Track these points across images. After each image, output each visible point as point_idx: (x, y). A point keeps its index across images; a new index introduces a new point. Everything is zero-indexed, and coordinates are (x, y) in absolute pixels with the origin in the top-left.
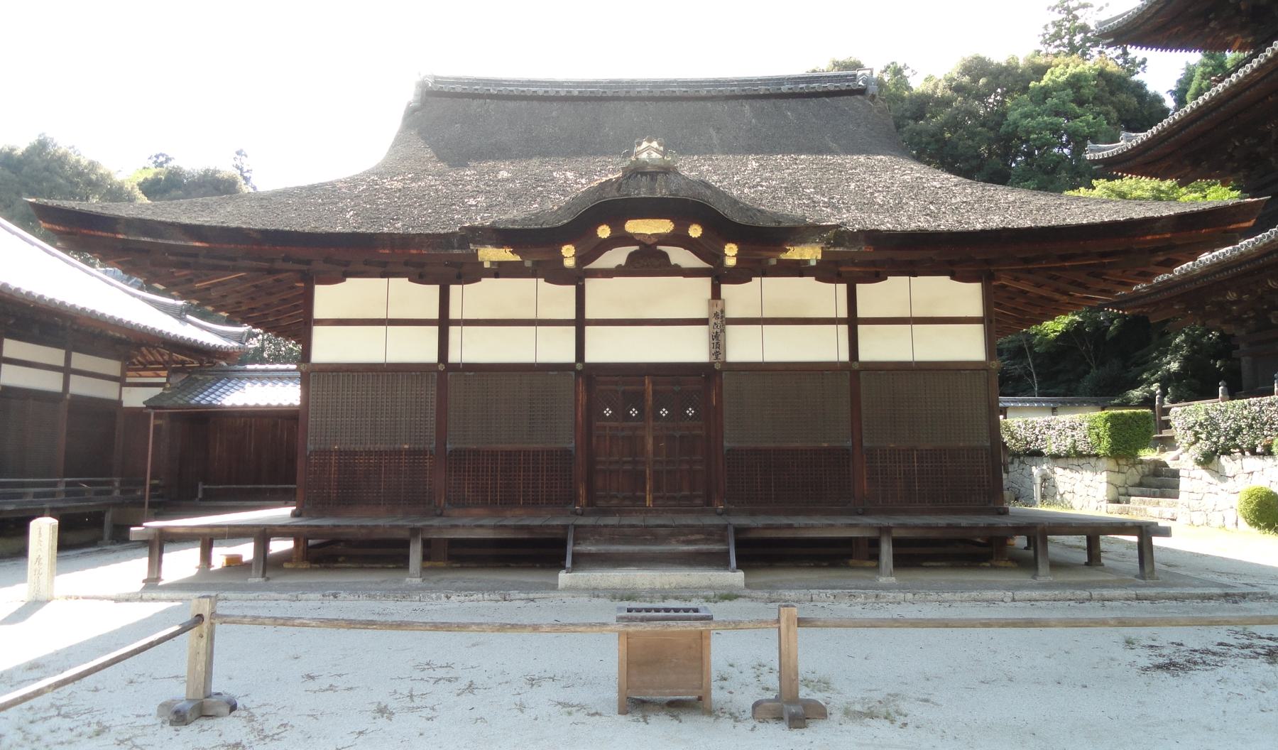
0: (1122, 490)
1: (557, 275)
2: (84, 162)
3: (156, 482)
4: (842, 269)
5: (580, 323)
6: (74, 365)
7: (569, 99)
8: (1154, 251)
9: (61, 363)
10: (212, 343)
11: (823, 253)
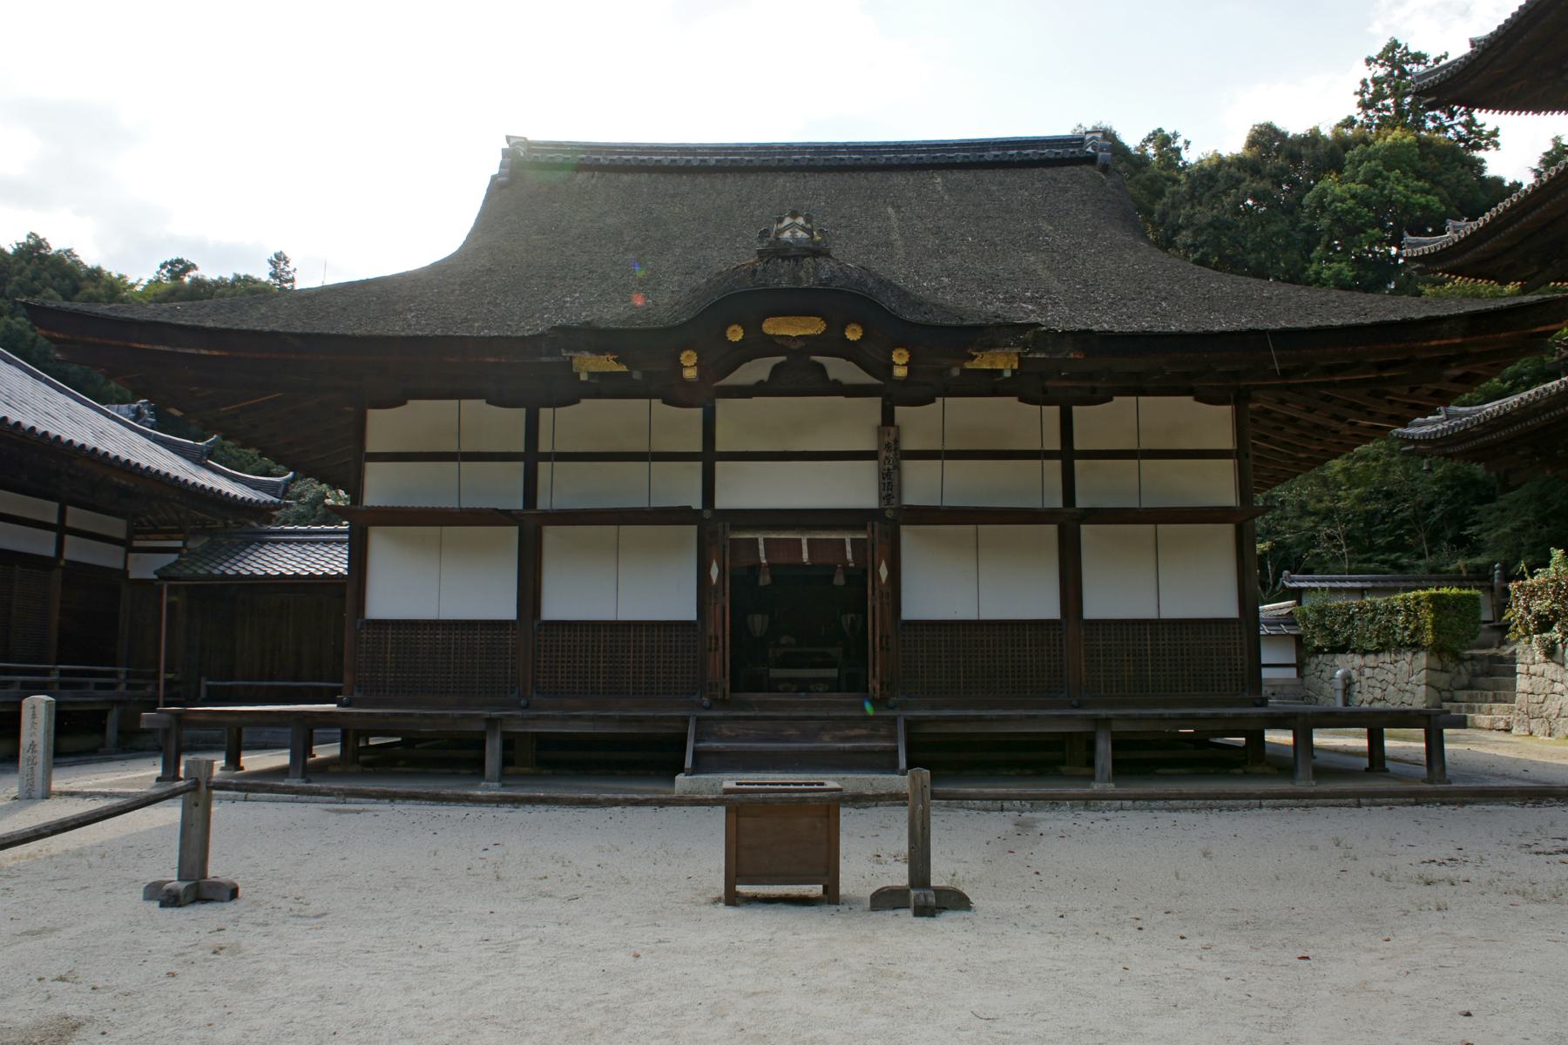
0: (1446, 695)
1: (678, 394)
2: (115, 275)
3: (170, 676)
4: (1048, 383)
5: (709, 457)
7: (705, 170)
8: (1445, 362)
10: (240, 496)
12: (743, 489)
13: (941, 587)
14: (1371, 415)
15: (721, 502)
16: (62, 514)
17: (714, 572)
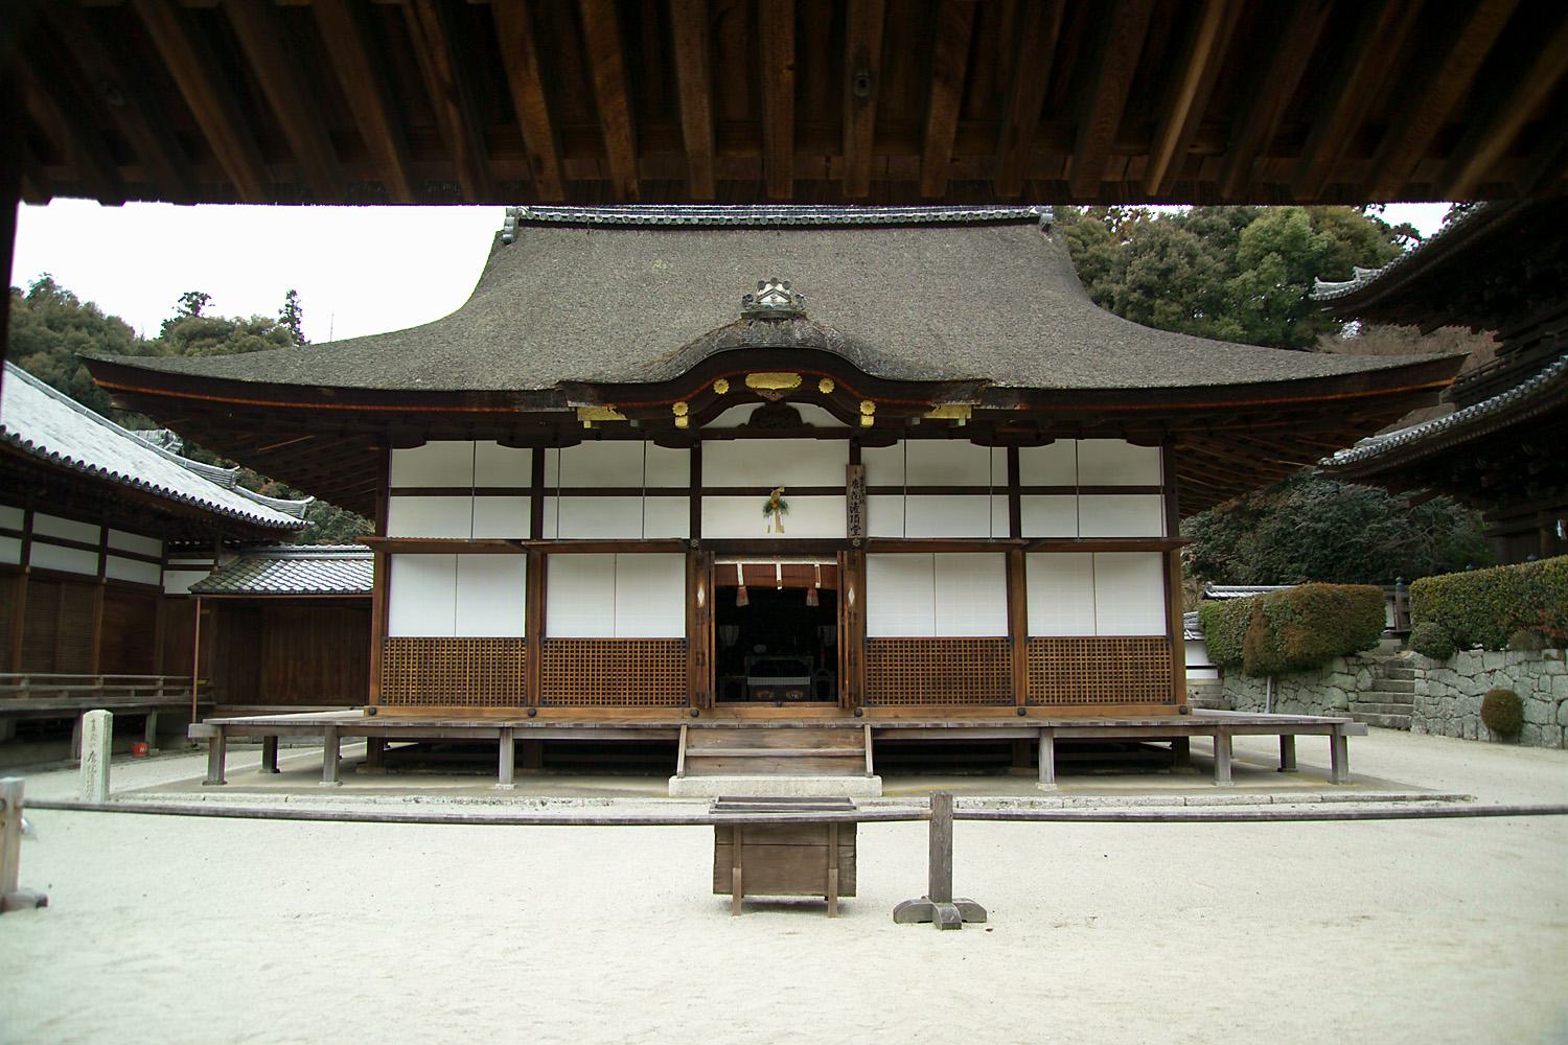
1: (669, 437)
3: (203, 682)
5: (696, 492)
6: (111, 544)
9: (19, 526)
11: (974, 412)
12: (730, 521)
13: (898, 609)
14: (1283, 456)
15: (707, 533)
16: (104, 537)
17: (701, 596)
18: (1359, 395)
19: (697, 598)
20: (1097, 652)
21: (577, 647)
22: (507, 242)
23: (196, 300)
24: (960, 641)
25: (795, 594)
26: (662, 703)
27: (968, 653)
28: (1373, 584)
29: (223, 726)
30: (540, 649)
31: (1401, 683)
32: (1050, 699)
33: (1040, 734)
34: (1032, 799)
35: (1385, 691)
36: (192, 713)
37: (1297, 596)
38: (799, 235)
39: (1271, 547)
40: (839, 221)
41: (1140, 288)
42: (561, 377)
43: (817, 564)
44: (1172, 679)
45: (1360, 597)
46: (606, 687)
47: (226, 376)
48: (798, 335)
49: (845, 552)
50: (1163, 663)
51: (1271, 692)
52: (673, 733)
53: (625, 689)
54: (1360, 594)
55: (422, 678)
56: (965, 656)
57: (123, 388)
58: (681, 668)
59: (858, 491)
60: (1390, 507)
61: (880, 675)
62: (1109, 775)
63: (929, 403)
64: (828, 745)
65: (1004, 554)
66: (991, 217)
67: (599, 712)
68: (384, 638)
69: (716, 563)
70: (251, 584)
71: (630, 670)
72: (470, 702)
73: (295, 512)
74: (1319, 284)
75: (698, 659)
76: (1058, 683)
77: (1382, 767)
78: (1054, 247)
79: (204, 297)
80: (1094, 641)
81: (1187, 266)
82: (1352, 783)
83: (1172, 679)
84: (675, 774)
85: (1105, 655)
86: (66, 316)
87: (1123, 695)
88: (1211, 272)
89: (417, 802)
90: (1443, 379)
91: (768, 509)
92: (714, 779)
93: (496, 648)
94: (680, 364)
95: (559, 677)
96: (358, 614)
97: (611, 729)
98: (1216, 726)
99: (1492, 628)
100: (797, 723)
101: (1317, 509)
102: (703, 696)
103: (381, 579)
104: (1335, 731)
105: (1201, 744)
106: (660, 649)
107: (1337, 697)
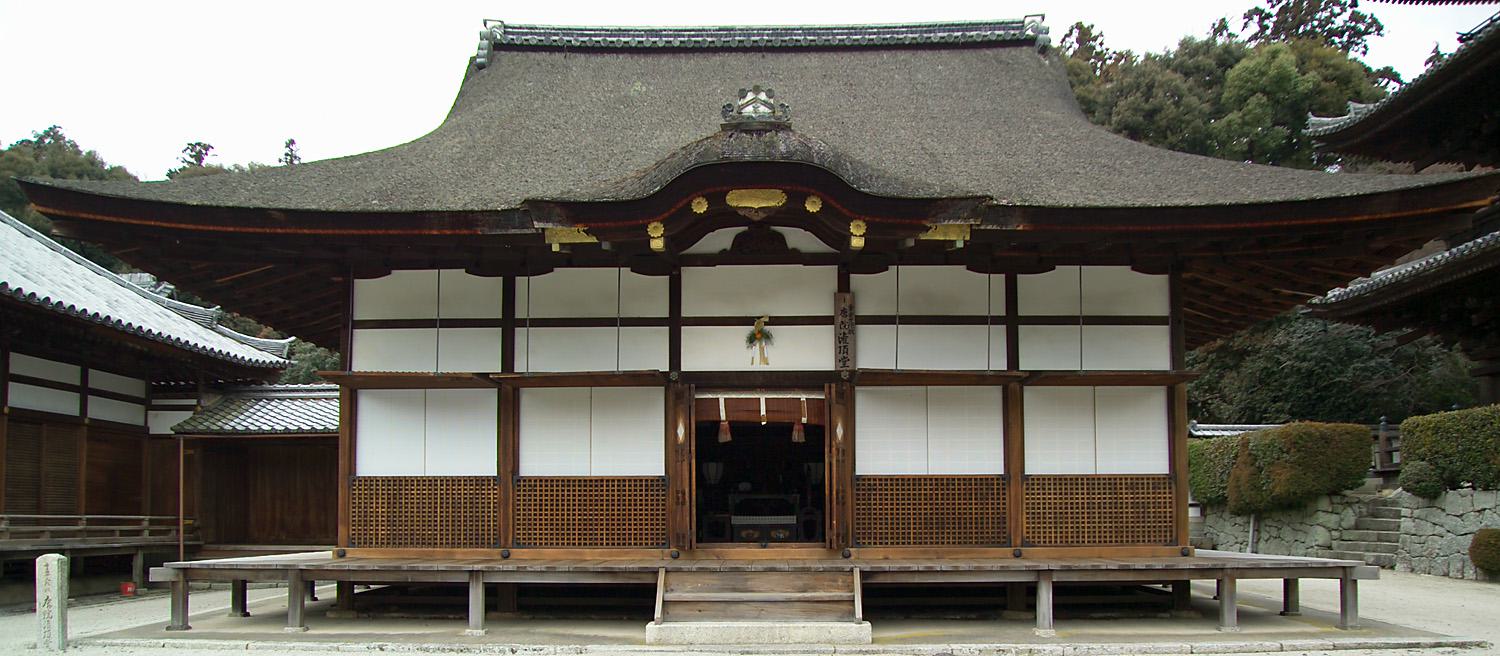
1: (646, 263)
5: (675, 323)
6: (92, 384)
12: (713, 352)
13: (889, 446)
14: (1294, 285)
15: (687, 366)
16: (85, 377)
17: (681, 431)
18: (1388, 216)
19: (676, 435)
20: (1097, 491)
21: (552, 486)
22: (481, 67)
23: (199, 151)
24: (954, 479)
25: (780, 430)
26: (641, 544)
27: (963, 492)
28: (1355, 422)
29: (185, 570)
30: (513, 487)
31: (1386, 522)
32: (1047, 540)
33: (1038, 577)
34: (1031, 646)
35: (1368, 529)
36: (179, 553)
37: (1285, 435)
38: (785, 57)
39: (1254, 387)
40: (827, 43)
41: (1125, 129)
42: (526, 196)
43: (803, 397)
44: (1174, 519)
45: (1348, 436)
46: (582, 527)
47: (170, 199)
48: (782, 148)
49: (833, 385)
50: (1165, 503)
51: (1254, 531)
52: (650, 576)
53: (602, 530)
54: (1348, 433)
55: (391, 519)
56: (959, 494)
57: (64, 213)
58: (660, 507)
59: (847, 319)
60: (1374, 346)
61: (869, 514)
62: (1115, 619)
63: (924, 222)
64: (814, 589)
65: (1000, 387)
66: (986, 39)
67: (577, 553)
68: (352, 477)
69: (697, 397)
70: (232, 424)
71: (607, 510)
72: (441, 544)
73: (277, 351)
74: (1313, 119)
75: (678, 498)
76: (1055, 523)
77: (1383, 610)
78: (1052, 70)
79: (207, 148)
80: (1094, 479)
81: (1173, 107)
82: (1361, 628)
83: (1174, 519)
84: (653, 620)
85: (1105, 494)
86: (68, 165)
87: (1123, 536)
88: (1196, 113)
89: (382, 649)
90: (1477, 200)
91: (752, 340)
92: (694, 625)
93: (468, 487)
94: (654, 180)
95: (533, 517)
96: (325, 453)
97: (585, 572)
98: (1222, 569)
99: (1485, 467)
100: (782, 566)
101: (1302, 348)
102: (684, 537)
103: (347, 415)
104: (1345, 575)
105: (1203, 588)
106: (638, 488)
107: (1320, 536)
